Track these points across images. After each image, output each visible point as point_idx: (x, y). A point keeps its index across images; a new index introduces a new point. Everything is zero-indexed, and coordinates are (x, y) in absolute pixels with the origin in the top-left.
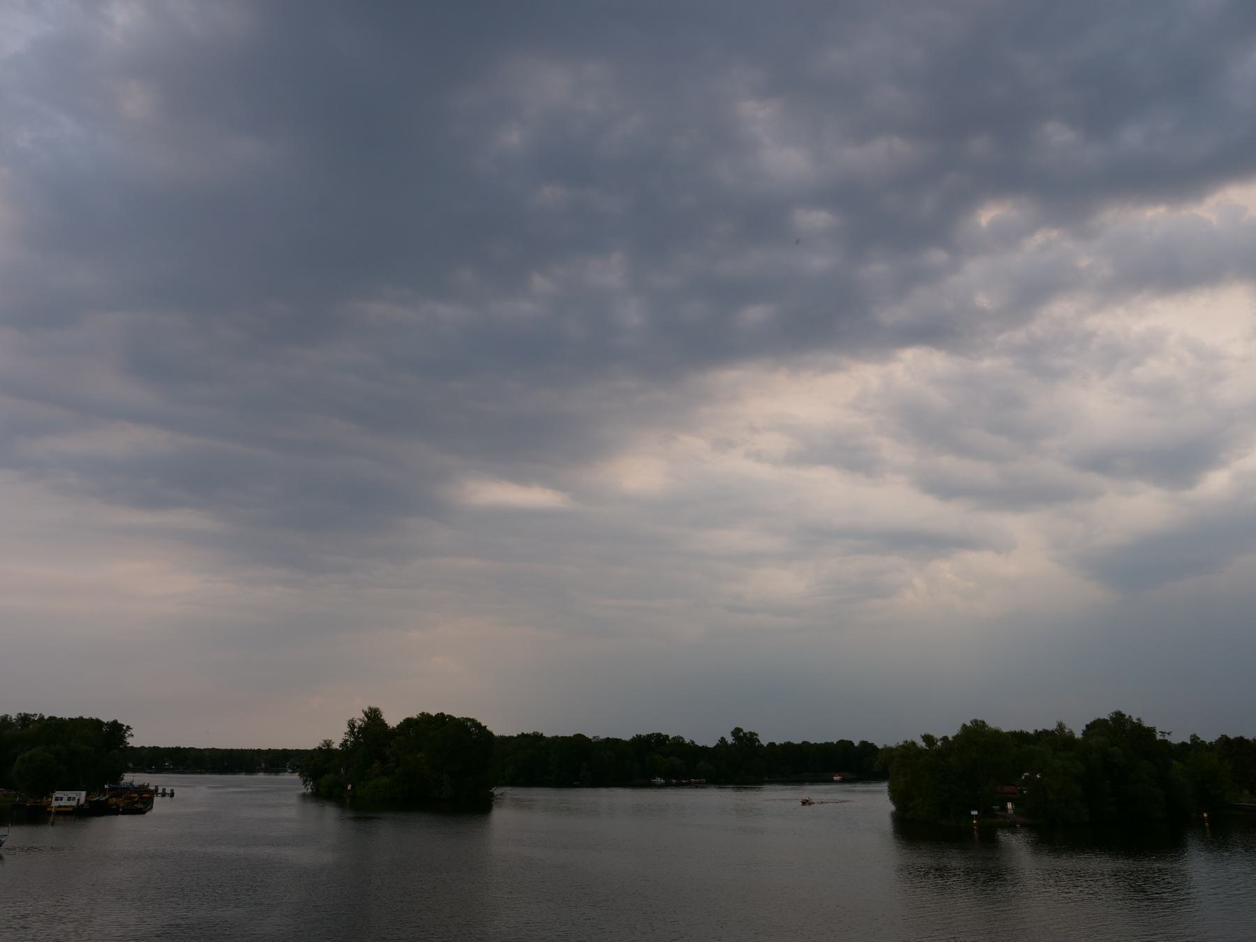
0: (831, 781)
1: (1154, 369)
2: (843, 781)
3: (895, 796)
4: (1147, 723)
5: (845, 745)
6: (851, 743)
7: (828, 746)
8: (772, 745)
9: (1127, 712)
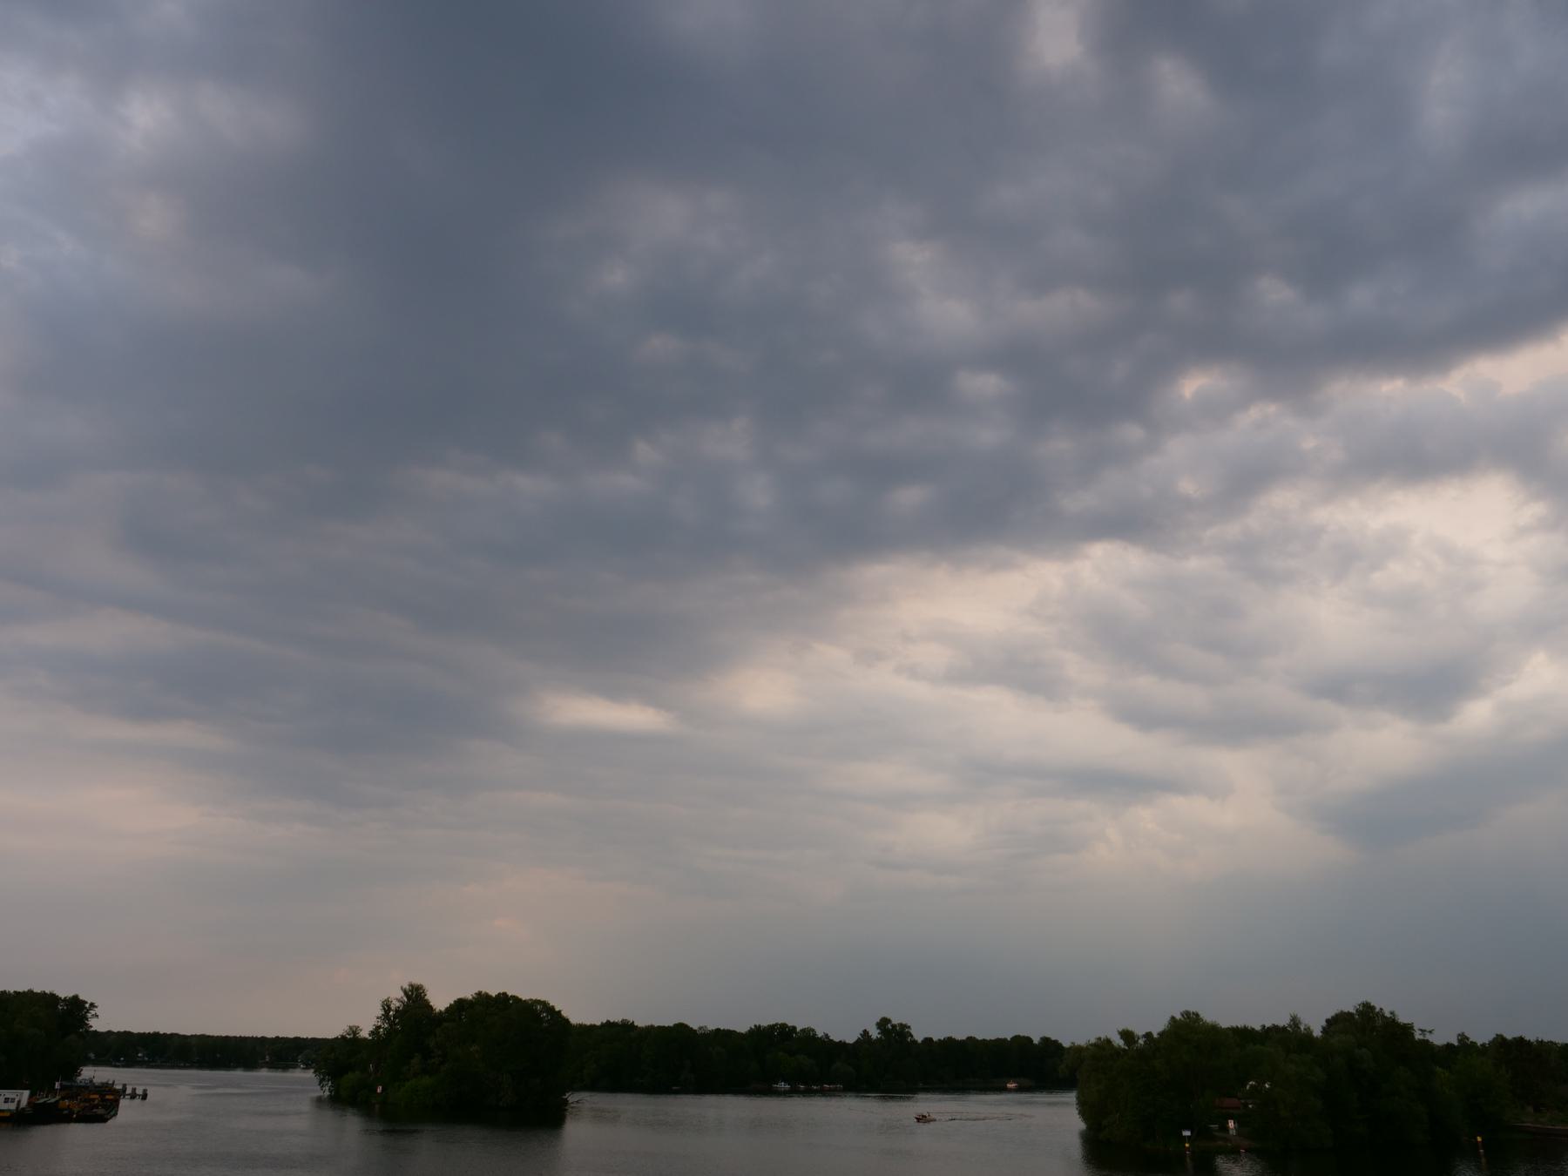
0: (1003, 1089)
1: (1397, 574)
2: (1020, 1090)
3: (1086, 1110)
4: (1403, 1019)
5: (1022, 1043)
6: (1029, 1040)
7: (1000, 1043)
8: (928, 1041)
9: (1377, 1004)
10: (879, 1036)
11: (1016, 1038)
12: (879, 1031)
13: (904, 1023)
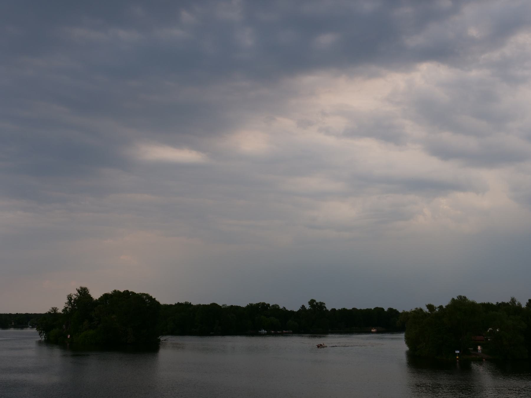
0: (369, 332)
2: (378, 332)
5: (379, 311)
6: (383, 309)
7: (368, 311)
10: (310, 308)
11: (376, 309)
12: (310, 306)
13: (322, 302)
